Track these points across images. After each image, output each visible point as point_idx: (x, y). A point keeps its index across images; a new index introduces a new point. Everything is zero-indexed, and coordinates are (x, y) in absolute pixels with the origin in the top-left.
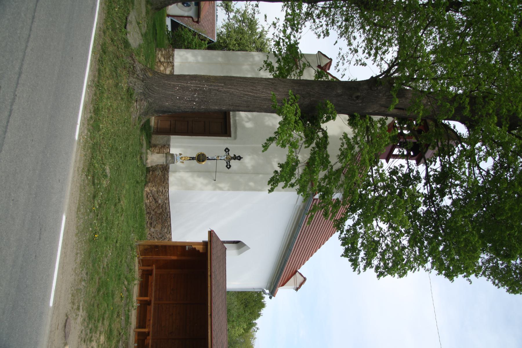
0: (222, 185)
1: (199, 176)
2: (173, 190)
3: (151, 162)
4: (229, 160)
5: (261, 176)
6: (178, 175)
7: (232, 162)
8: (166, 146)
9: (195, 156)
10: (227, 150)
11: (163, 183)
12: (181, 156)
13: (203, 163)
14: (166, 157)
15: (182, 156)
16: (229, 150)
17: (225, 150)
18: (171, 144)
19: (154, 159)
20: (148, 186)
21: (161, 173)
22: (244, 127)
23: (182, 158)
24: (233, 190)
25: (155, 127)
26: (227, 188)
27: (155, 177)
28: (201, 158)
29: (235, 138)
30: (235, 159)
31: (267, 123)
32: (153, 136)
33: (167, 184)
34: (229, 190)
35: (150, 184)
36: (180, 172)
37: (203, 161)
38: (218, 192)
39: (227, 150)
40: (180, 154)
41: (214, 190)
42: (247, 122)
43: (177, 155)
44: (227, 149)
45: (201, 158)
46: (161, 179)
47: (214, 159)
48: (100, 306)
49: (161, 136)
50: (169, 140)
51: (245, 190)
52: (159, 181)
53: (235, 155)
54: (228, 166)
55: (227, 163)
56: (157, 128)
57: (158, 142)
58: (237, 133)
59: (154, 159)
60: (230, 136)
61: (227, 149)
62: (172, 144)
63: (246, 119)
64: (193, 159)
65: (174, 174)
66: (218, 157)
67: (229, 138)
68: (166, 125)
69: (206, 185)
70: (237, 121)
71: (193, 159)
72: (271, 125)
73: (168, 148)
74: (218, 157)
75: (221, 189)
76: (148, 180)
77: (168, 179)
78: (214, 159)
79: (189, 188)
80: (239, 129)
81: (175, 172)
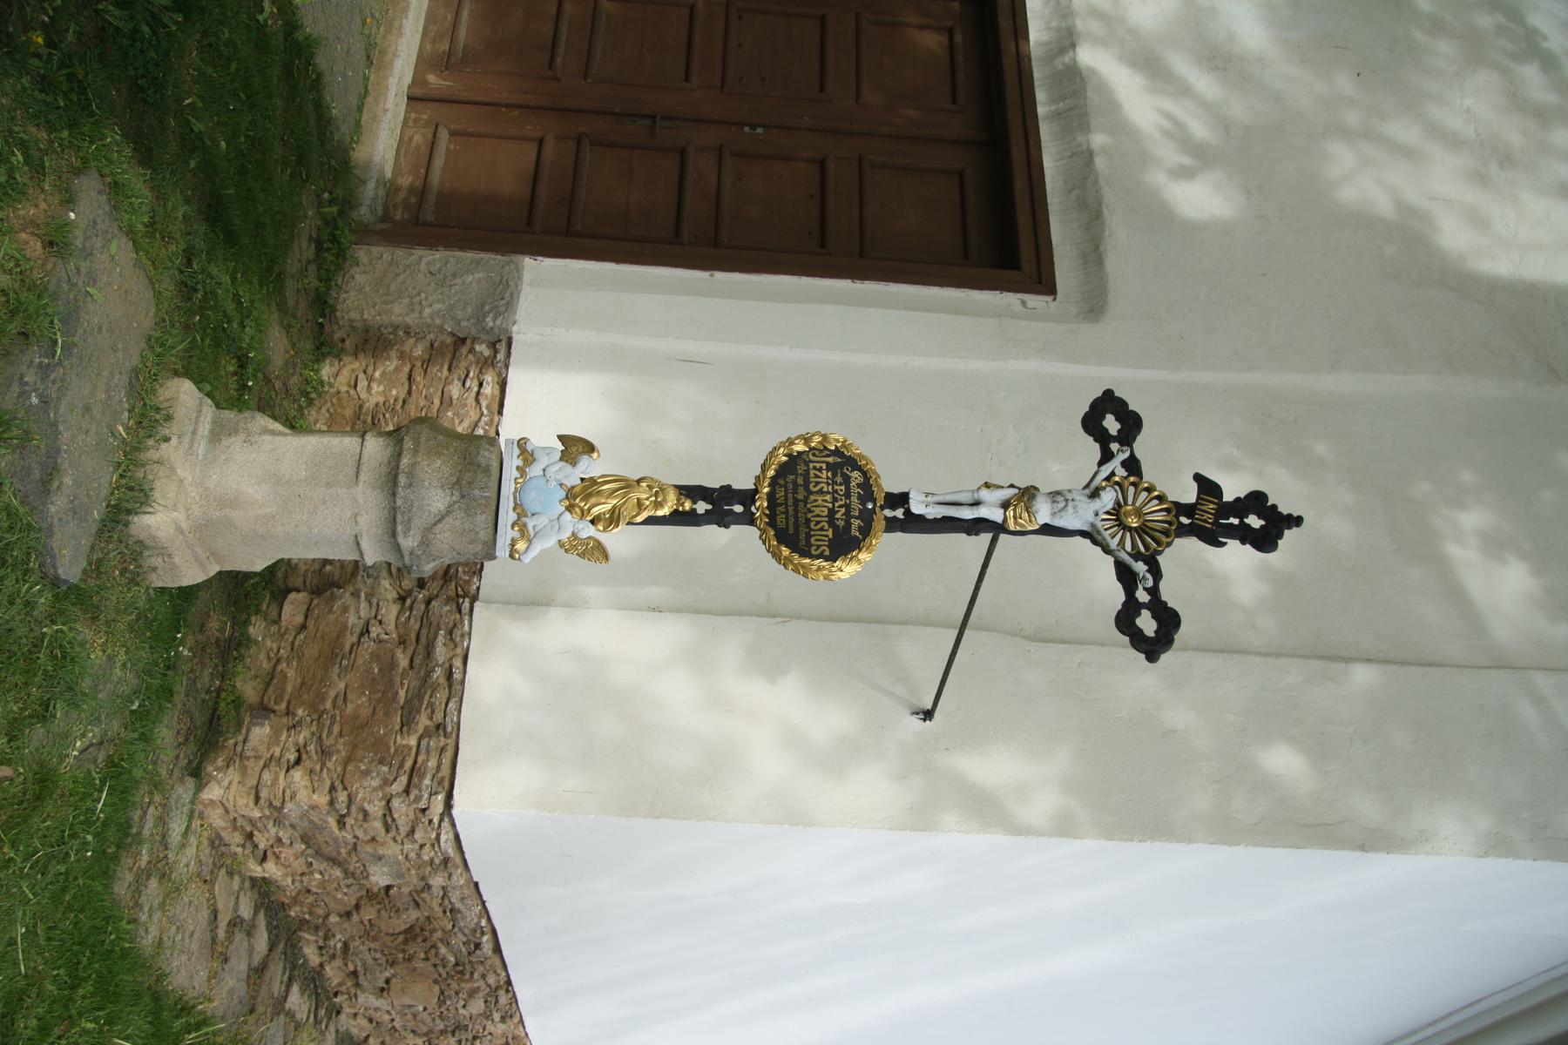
0: (993, 767)
1: (767, 665)
2: (493, 800)
3: (204, 531)
4: (1145, 534)
5: (1363, 676)
6: (554, 634)
7: (1188, 567)
8: (481, 347)
9: (743, 481)
10: (1113, 423)
11: (407, 724)
12: (573, 476)
13: (846, 570)
14: (391, 480)
15: (590, 467)
16: (1132, 424)
17: (1091, 423)
18: (524, 332)
19: (240, 489)
20: (237, 758)
21: (390, 612)
22: (1159, 217)
23: (590, 487)
24: (1109, 833)
25: (405, 181)
26: (1042, 805)
27: (332, 655)
28: (813, 507)
29: (1094, 306)
30: (1212, 537)
31: (1348, 194)
32: (362, 253)
33: (446, 733)
34: (1063, 827)
35: (260, 733)
36: (572, 605)
37: (844, 545)
38: (960, 842)
39: (1113, 423)
40: (575, 447)
41: (920, 818)
42: (1184, 173)
43: (527, 454)
44: (1108, 402)
45: (821, 505)
46: (381, 683)
47: (976, 526)
48: (361, 817)
49: (430, 258)
50: (503, 297)
51: (1226, 831)
52: (359, 703)
53: (1207, 487)
54: (1147, 623)
55: (1126, 576)
56: (422, 192)
57: (399, 312)
58: (1111, 265)
59: (240, 489)
60: (1044, 283)
61: (1108, 402)
62: (529, 324)
63: (1171, 155)
64: (717, 505)
65: (517, 632)
66: (1027, 495)
67: (1036, 301)
68: (503, 167)
69: (836, 759)
70: (1100, 163)
71: (717, 505)
72: (1383, 206)
73: (486, 363)
74: (1027, 495)
75: (985, 808)
76: (249, 690)
77: (454, 685)
78: (976, 526)
79: (659, 789)
80: (1119, 231)
81: (533, 603)
